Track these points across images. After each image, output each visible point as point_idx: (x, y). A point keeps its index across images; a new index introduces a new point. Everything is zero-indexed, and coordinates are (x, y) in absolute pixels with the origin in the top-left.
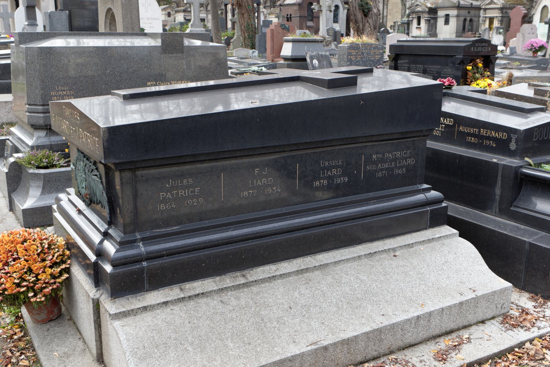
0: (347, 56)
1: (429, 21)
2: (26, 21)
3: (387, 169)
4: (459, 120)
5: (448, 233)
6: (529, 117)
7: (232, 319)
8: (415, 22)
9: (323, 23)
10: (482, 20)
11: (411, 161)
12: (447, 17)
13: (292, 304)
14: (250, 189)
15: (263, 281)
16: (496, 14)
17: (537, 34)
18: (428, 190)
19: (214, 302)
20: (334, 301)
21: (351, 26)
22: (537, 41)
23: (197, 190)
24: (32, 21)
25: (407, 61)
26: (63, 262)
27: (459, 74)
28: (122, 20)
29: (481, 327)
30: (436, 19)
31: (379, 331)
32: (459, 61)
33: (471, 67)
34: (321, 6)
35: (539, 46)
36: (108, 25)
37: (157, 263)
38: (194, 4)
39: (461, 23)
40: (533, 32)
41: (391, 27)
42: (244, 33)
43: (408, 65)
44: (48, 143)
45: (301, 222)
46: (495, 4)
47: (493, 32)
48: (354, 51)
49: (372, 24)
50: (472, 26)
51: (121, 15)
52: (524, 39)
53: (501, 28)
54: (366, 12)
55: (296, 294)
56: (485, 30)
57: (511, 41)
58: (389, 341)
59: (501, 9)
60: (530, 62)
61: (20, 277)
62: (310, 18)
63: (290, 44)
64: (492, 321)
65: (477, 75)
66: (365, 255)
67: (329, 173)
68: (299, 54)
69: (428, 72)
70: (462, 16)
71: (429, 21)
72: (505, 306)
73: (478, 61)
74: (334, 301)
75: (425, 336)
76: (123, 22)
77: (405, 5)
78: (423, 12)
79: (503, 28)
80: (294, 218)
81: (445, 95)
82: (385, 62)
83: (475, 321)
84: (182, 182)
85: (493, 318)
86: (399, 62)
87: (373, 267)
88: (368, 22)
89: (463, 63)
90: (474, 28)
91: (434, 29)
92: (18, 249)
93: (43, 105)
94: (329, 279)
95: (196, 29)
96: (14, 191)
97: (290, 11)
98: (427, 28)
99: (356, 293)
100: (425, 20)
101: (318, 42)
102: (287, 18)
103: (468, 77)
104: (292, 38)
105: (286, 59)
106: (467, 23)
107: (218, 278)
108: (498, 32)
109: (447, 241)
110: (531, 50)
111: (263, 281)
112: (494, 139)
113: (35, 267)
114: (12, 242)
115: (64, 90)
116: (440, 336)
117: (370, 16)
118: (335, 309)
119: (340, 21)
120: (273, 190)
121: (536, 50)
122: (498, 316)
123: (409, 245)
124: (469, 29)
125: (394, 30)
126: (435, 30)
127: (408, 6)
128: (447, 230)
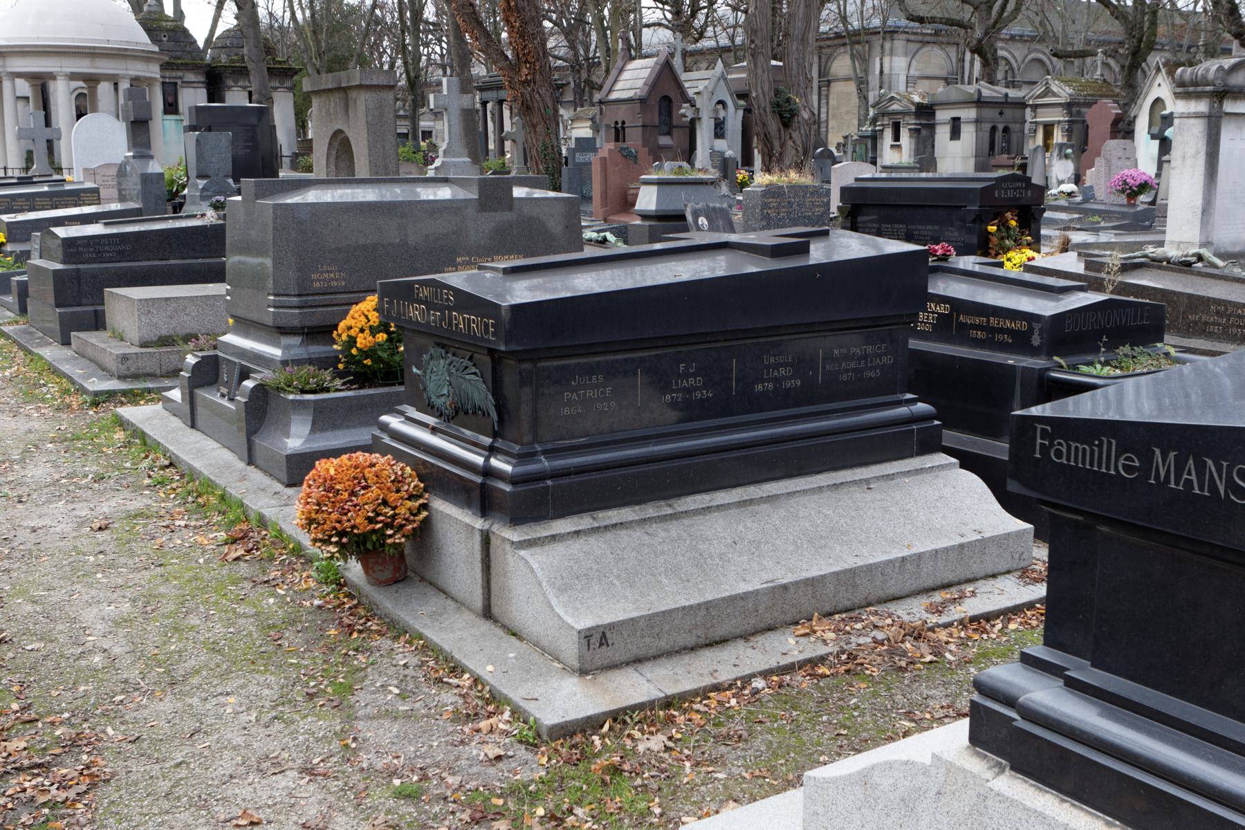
0: (762, 210)
1: (917, 131)
2: (129, 150)
3: (854, 370)
4: (958, 305)
5: (944, 462)
6: (1062, 299)
7: (664, 552)
8: (888, 135)
9: (703, 143)
10: (1030, 130)
11: (887, 360)
12: (956, 125)
13: (737, 539)
14: (674, 391)
15: (696, 512)
16: (1057, 116)
17: (1136, 160)
18: (913, 401)
19: (637, 534)
20: (791, 538)
21: (754, 145)
22: (1135, 174)
23: (608, 390)
24: (143, 150)
25: (875, 217)
26: (421, 496)
27: (974, 240)
28: (367, 152)
29: (992, 582)
30: (932, 128)
31: (853, 572)
32: (973, 217)
33: (995, 228)
34: (698, 110)
35: (1137, 183)
36: (332, 160)
37: (564, 481)
38: (449, 110)
39: (987, 136)
40: (1127, 155)
41: (838, 146)
42: (537, 164)
43: (877, 226)
44: (306, 356)
45: (741, 439)
46: (1055, 95)
47: (1051, 155)
48: (774, 200)
49: (799, 142)
50: (1008, 142)
51: (365, 142)
52: (1110, 170)
53: (1067, 146)
54: (786, 116)
55: (741, 528)
56: (1036, 149)
57: (1088, 172)
58: (866, 589)
59: (1068, 106)
60: (1123, 216)
61: (374, 511)
62: (666, 129)
63: (654, 189)
64: (1007, 576)
65: (1007, 242)
66: (828, 486)
67: (776, 373)
68: (672, 206)
69: (916, 237)
70: (986, 122)
71: (917, 131)
72: (1024, 556)
73: (1009, 215)
74: (791, 538)
75: (913, 588)
76: (370, 156)
77: (866, 98)
78: (903, 113)
79: (1072, 147)
80: (732, 433)
81: (936, 270)
82: (831, 219)
83: (982, 574)
84: (590, 380)
85: (1008, 572)
86: (860, 219)
87: (840, 500)
88: (791, 138)
89: (981, 219)
90: (1014, 147)
91: (929, 149)
92: (367, 475)
93: (299, 295)
94: (782, 512)
95: (453, 159)
96: (255, 432)
97: (622, 114)
98: (913, 147)
99: (819, 529)
100: (910, 130)
101: (706, 183)
102: (617, 130)
103: (991, 246)
104: (656, 177)
105: (645, 216)
106: (999, 135)
107: (637, 508)
108: (1063, 154)
109: (942, 473)
110: (1123, 191)
111: (696, 512)
112: (1010, 332)
113: (392, 497)
114: (356, 467)
115: (331, 272)
116: (934, 589)
117: (795, 125)
118: (792, 548)
119: (729, 134)
120: (702, 394)
121: (1134, 191)
122: (1016, 570)
123: (888, 475)
124: (1003, 148)
125: (845, 152)
126: (930, 150)
127: (871, 101)
128: (942, 459)
